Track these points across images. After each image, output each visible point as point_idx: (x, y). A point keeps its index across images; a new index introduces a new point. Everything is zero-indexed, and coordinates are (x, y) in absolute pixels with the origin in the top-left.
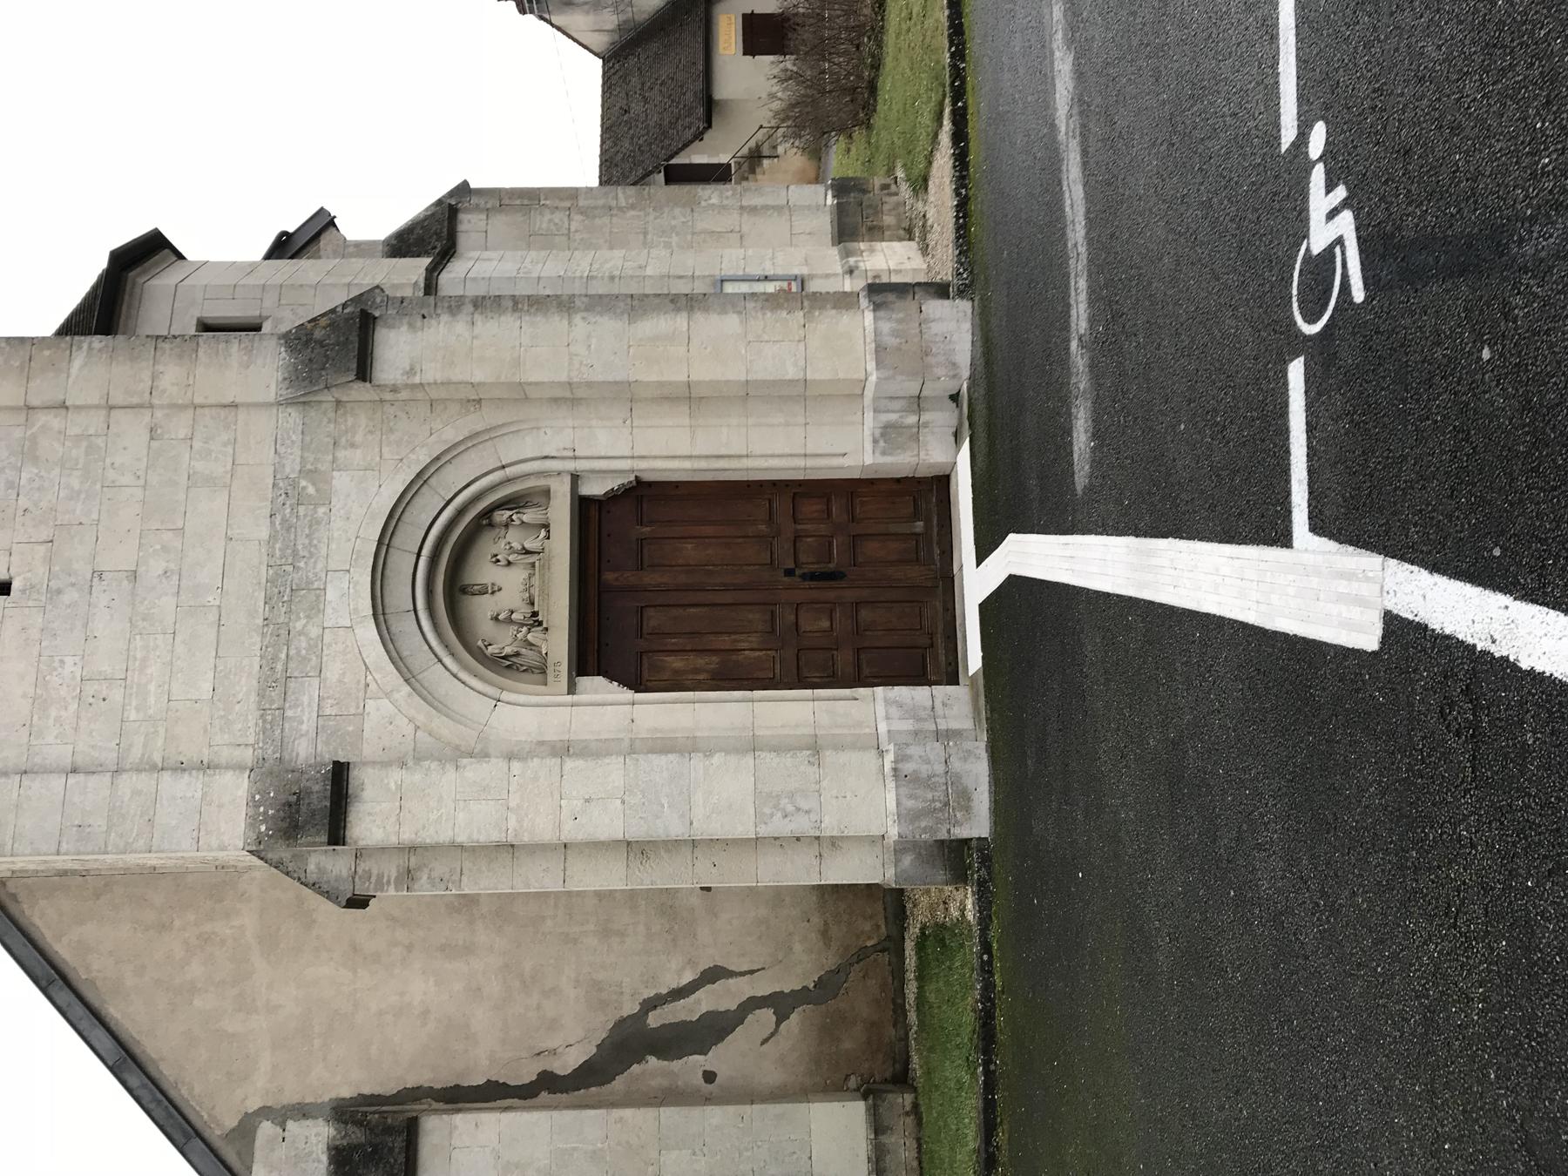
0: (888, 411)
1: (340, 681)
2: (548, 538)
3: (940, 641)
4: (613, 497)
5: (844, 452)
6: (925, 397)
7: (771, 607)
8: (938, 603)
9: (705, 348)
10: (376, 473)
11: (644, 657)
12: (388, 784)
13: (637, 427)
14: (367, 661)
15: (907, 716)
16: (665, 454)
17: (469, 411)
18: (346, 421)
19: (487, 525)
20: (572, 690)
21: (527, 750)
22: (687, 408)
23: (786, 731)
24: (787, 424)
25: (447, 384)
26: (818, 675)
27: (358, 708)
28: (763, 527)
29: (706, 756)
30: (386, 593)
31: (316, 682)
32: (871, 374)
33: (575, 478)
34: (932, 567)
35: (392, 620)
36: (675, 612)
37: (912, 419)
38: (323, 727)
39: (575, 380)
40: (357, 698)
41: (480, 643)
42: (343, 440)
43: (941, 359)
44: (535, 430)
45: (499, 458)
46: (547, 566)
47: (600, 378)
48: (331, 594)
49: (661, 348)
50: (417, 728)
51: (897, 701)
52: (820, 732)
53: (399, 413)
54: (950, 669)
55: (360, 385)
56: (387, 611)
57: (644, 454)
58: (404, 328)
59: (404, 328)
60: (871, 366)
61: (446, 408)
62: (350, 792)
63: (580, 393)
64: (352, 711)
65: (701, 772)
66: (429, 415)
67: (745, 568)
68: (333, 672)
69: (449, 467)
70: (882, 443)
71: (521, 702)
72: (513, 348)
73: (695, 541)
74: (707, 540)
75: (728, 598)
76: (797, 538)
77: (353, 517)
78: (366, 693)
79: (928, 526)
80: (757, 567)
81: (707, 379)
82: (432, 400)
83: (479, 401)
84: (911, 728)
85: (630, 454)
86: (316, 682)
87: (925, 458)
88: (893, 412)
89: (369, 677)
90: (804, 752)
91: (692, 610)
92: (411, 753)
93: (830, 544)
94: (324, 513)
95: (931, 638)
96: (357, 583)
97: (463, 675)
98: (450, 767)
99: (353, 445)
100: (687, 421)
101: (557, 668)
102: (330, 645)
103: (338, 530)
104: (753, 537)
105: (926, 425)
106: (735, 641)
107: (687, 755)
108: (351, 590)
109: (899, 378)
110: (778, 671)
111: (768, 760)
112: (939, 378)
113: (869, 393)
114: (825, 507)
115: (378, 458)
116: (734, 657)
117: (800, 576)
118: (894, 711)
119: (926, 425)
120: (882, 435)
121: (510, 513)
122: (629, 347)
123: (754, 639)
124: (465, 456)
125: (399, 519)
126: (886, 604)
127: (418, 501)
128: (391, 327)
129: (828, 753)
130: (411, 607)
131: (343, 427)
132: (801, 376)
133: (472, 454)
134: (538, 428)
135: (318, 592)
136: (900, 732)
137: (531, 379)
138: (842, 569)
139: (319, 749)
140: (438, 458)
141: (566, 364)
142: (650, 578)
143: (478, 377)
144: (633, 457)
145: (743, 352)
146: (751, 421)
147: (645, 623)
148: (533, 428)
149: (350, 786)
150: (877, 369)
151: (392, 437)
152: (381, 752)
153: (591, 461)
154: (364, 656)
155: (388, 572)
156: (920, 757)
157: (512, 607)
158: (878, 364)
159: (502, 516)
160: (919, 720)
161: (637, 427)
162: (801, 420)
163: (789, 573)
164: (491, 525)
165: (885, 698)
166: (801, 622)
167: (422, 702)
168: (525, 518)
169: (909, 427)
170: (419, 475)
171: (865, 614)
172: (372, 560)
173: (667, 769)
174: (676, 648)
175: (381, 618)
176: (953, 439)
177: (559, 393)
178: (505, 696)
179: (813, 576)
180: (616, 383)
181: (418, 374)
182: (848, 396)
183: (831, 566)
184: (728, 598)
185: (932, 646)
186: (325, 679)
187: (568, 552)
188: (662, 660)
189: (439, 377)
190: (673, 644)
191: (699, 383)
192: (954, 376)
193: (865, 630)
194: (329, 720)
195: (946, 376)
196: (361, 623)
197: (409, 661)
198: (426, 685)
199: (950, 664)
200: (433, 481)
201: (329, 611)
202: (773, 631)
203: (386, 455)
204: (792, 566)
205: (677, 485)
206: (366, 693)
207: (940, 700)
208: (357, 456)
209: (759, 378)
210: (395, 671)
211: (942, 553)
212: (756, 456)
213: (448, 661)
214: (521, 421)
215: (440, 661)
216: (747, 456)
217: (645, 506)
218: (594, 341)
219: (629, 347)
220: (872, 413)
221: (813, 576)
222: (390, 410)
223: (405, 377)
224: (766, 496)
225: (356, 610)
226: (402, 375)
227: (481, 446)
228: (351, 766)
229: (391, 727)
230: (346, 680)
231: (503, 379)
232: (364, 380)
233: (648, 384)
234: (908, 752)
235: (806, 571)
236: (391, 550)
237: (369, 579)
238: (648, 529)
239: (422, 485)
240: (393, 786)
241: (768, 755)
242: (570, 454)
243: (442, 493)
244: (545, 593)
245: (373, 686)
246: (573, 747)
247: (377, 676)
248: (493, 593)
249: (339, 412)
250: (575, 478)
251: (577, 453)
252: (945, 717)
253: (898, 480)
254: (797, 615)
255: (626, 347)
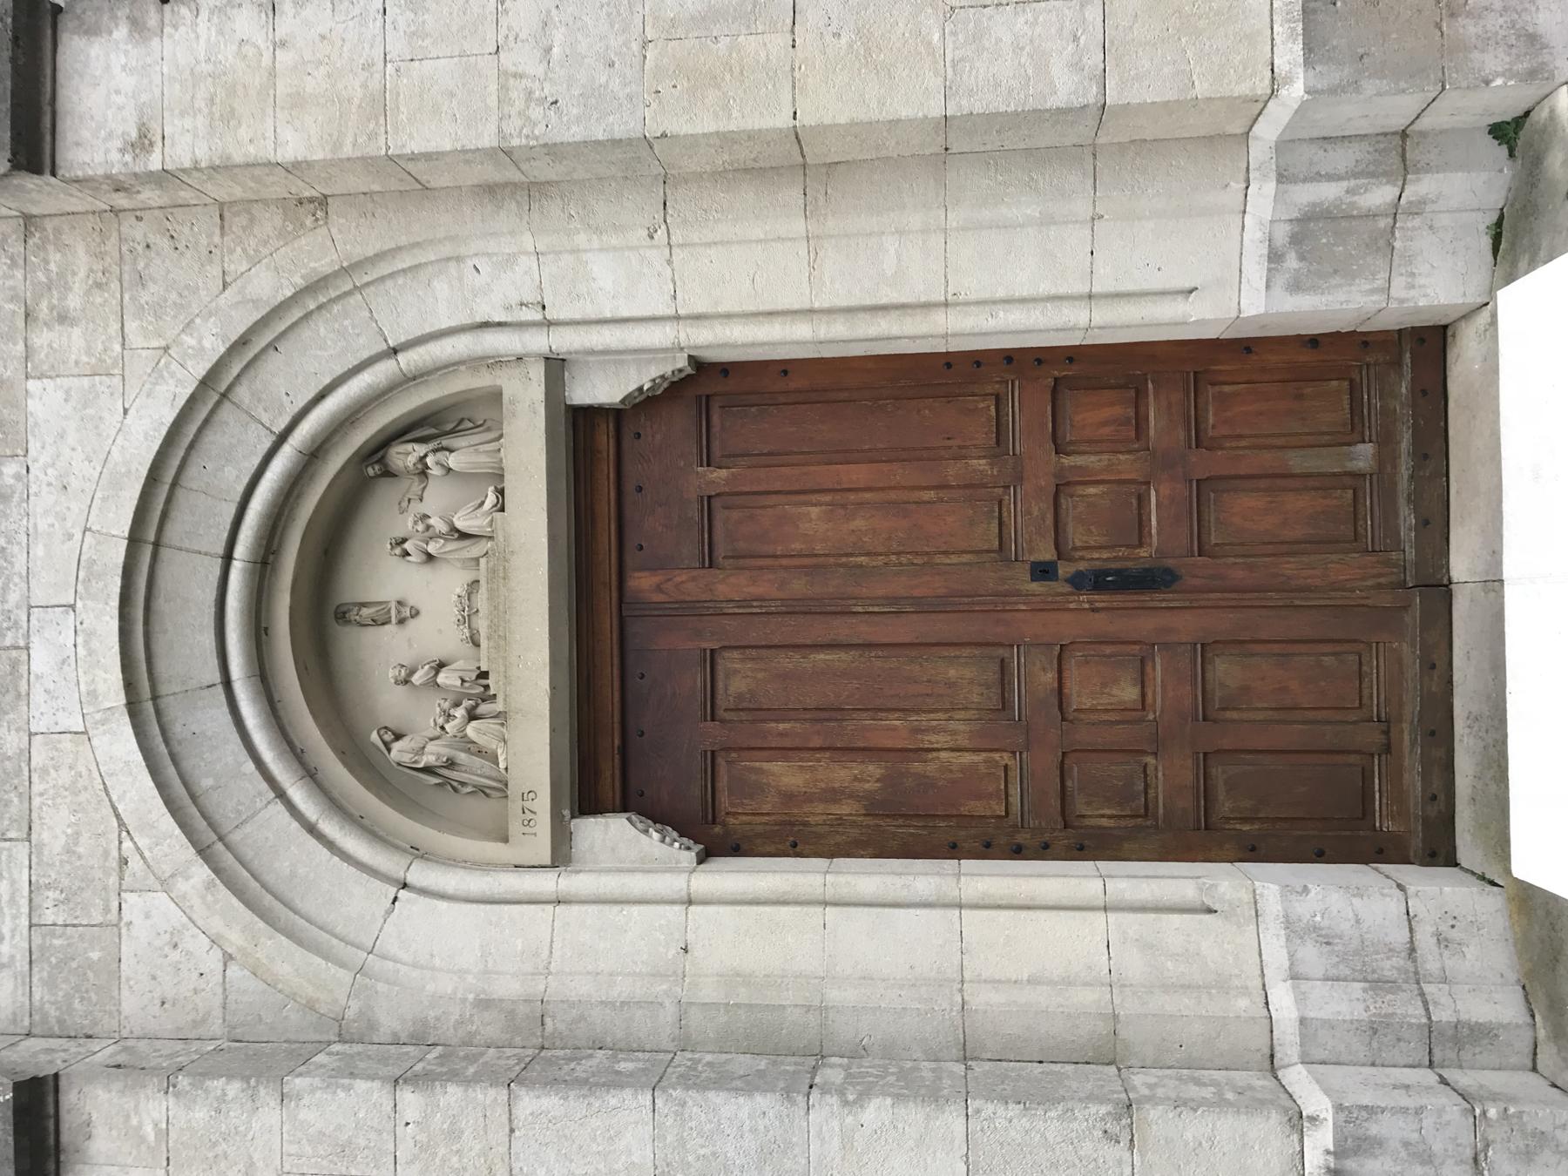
0: (1318, 177)
1: (69, 851)
2: (502, 510)
3: (1407, 738)
4: (645, 404)
5: (1188, 285)
6: (1423, 134)
7: (1001, 652)
8: (1406, 648)
9: (837, 35)
10: (117, 380)
11: (720, 761)
12: (140, 1126)
13: (681, 246)
14: (121, 809)
15: (1344, 971)
16: (751, 307)
17: (302, 225)
18: (46, 262)
19: (377, 476)
20: (562, 855)
21: (454, 1018)
22: (796, 193)
23: (1041, 997)
24: (1047, 221)
25: (222, 168)
26: (1108, 812)
27: (107, 910)
28: (981, 464)
29: (846, 1103)
30: (159, 647)
31: (21, 851)
32: (1289, 80)
33: (556, 367)
34: (1394, 555)
35: (175, 710)
36: (787, 662)
37: (1380, 195)
38: (42, 948)
39: (515, 142)
40: (105, 888)
41: (374, 736)
42: (44, 305)
43: (1494, 22)
44: (452, 264)
45: (383, 334)
46: (500, 574)
47: (576, 133)
48: (41, 660)
49: (724, 42)
50: (228, 958)
51: (1316, 928)
52: (1128, 1006)
53: (152, 239)
54: (1433, 811)
55: (30, 182)
56: (163, 689)
57: (700, 308)
58: (121, 32)
59: (121, 32)
60: (1289, 54)
61: (252, 220)
62: (65, 1138)
63: (544, 170)
64: (98, 919)
65: (836, 1142)
66: (217, 239)
67: (939, 559)
68: (54, 829)
69: (274, 362)
70: (1292, 262)
71: (450, 890)
72: (368, 66)
73: (827, 498)
74: (852, 497)
75: (902, 630)
76: (1060, 489)
77: (75, 484)
78: (121, 878)
79: (1386, 456)
80: (966, 558)
81: (843, 119)
82: (221, 205)
83: (323, 202)
84: (1359, 1013)
85: (671, 312)
86: (21, 851)
87: (1403, 294)
88: (1330, 178)
89: (127, 844)
90: (1093, 1109)
91: (822, 656)
92: (218, 1012)
93: (1142, 500)
94: (17, 477)
95: (1387, 733)
96: (90, 634)
97: (330, 828)
98: (267, 1095)
99: (63, 318)
100: (799, 226)
101: (527, 804)
102: (44, 771)
103: (46, 512)
104: (959, 487)
105: (1417, 209)
106: (917, 731)
107: (801, 1099)
108: (81, 651)
109: (1370, 86)
110: (1015, 800)
111: (1000, 1123)
112: (1487, 83)
113: (1268, 131)
114: (1131, 412)
115: (118, 348)
116: (917, 767)
117: (1067, 581)
118: (1312, 956)
119: (1417, 209)
120: (1296, 240)
121: (421, 449)
122: (645, 44)
123: (961, 727)
124: (305, 333)
125: (175, 484)
126: (1276, 648)
127: (215, 440)
128: (92, 31)
129: (1153, 1113)
130: (216, 677)
131: (41, 276)
132: (1091, 96)
133: (321, 328)
134: (459, 259)
135: (14, 653)
136: (1330, 1025)
137: (415, 147)
138: (1170, 563)
139: (37, 997)
140: (243, 342)
141: (493, 101)
142: (730, 586)
143: (292, 147)
144: (677, 318)
145: (936, 37)
146: (954, 218)
147: (720, 685)
148: (449, 259)
149: (64, 1127)
150: (1308, 63)
151: (145, 297)
152: (156, 1009)
153: (582, 330)
154: (114, 798)
155: (160, 604)
156: (1406, 1144)
157: (437, 654)
158: (1308, 49)
159: (405, 455)
160: (1378, 984)
161: (681, 246)
162: (1082, 208)
163: (1043, 572)
164: (388, 474)
165: (1286, 916)
166: (1072, 687)
167: (235, 901)
168: (453, 461)
169: (1371, 215)
170: (206, 382)
171: (1226, 672)
172: (118, 581)
173: (754, 1130)
174: (787, 743)
175: (149, 707)
176: (1486, 242)
177: (491, 174)
178: (420, 874)
179: (1098, 581)
180: (616, 143)
181: (158, 149)
182: (1209, 140)
183: (1143, 552)
184: (902, 630)
185: (1387, 748)
186: (41, 846)
187: (545, 540)
188: (760, 771)
189: (203, 154)
190: (782, 735)
191: (822, 130)
192: (1532, 74)
193: (1224, 709)
194: (53, 935)
195: (1509, 74)
196: (103, 722)
197: (212, 801)
198: (249, 854)
199: (1434, 798)
200: (242, 393)
201: (38, 696)
202: (1005, 704)
203: (135, 340)
204: (1046, 554)
205: (785, 368)
206: (121, 878)
207: (1430, 929)
208: (74, 339)
209: (978, 108)
210: (178, 831)
211: (1424, 523)
212: (967, 304)
213: (297, 794)
214: (417, 245)
215: (281, 795)
216: (946, 304)
217: (715, 419)
218: (558, 37)
219: (645, 44)
220: (1271, 187)
221: (1098, 581)
222: (138, 232)
223: (128, 158)
224: (989, 389)
225: (93, 694)
226: (122, 151)
227: (336, 308)
228: (63, 1083)
229: (175, 956)
230: (81, 850)
231: (347, 151)
232: (36, 169)
233: (693, 141)
234: (1374, 1129)
235: (1082, 566)
236: (165, 553)
237: (114, 625)
238: (723, 473)
239: (218, 404)
240: (149, 1130)
241: (1001, 1110)
242: (536, 316)
243: (265, 418)
244: (501, 638)
245: (135, 864)
246: (553, 1018)
247: (142, 842)
248: (401, 622)
249: (31, 242)
250: (556, 367)
251: (551, 314)
252: (1445, 980)
253: (1314, 341)
254: (1060, 672)
255: (635, 47)
